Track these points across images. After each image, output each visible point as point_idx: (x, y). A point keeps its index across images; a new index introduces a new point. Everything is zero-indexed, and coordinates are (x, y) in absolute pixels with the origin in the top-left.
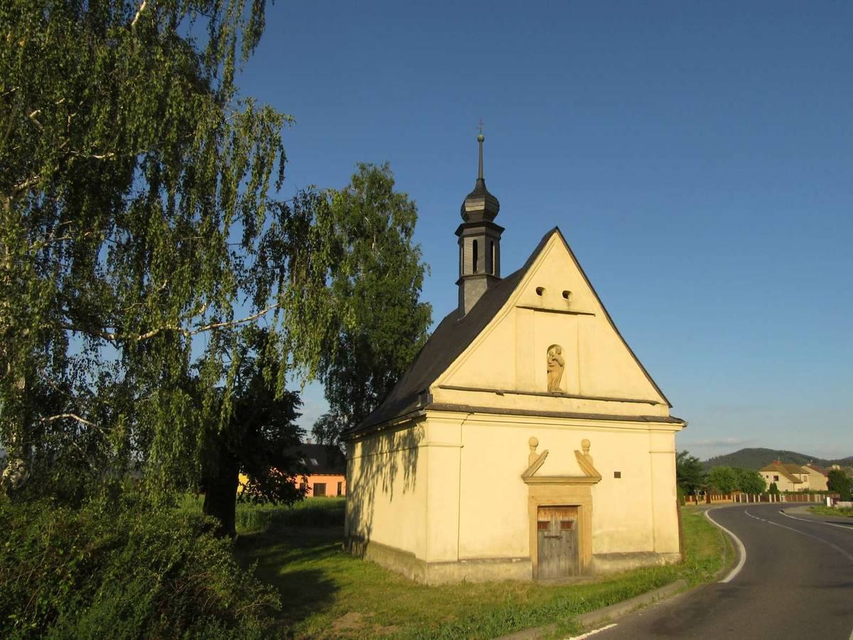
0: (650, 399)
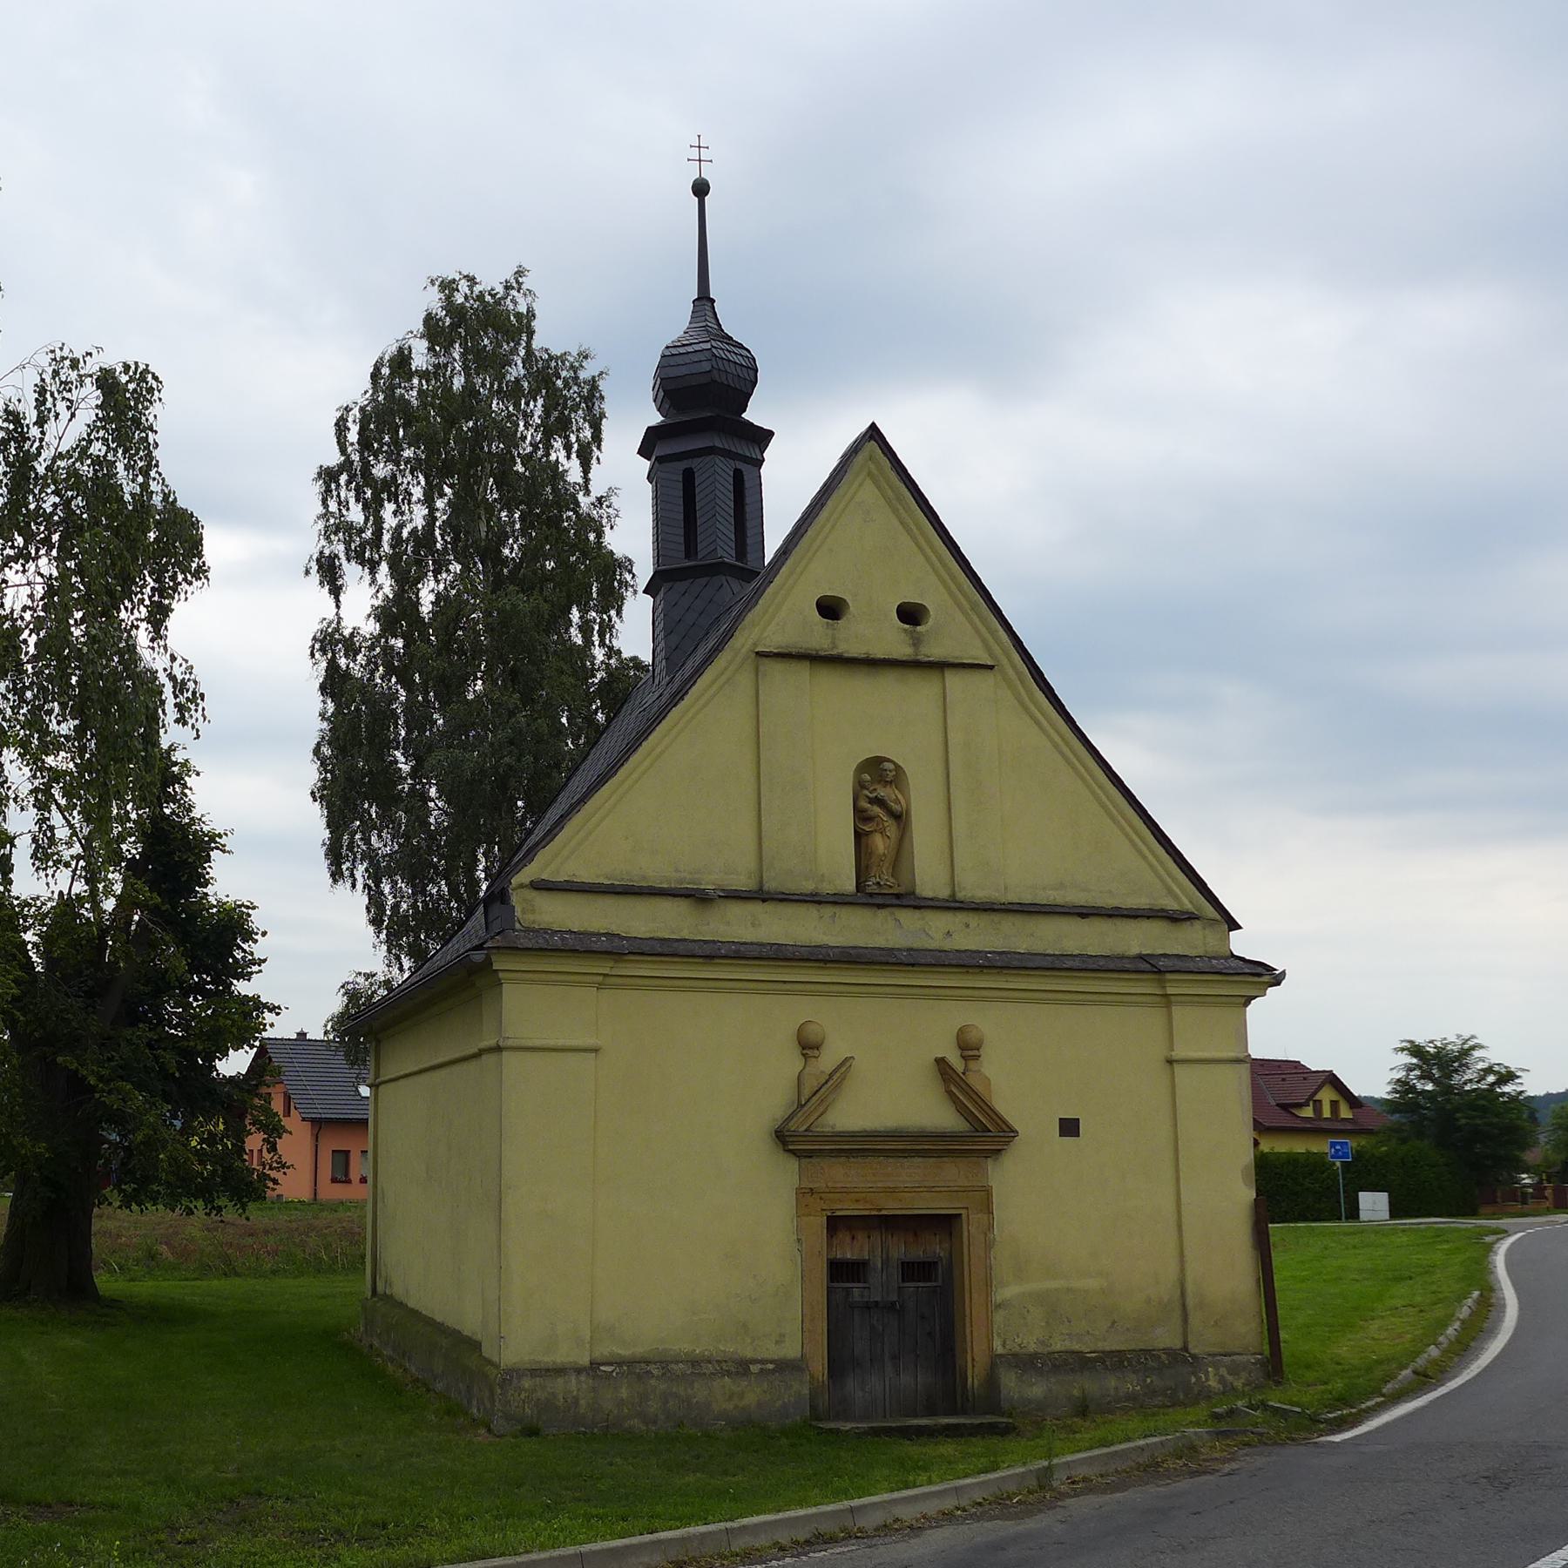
0: (1170, 904)
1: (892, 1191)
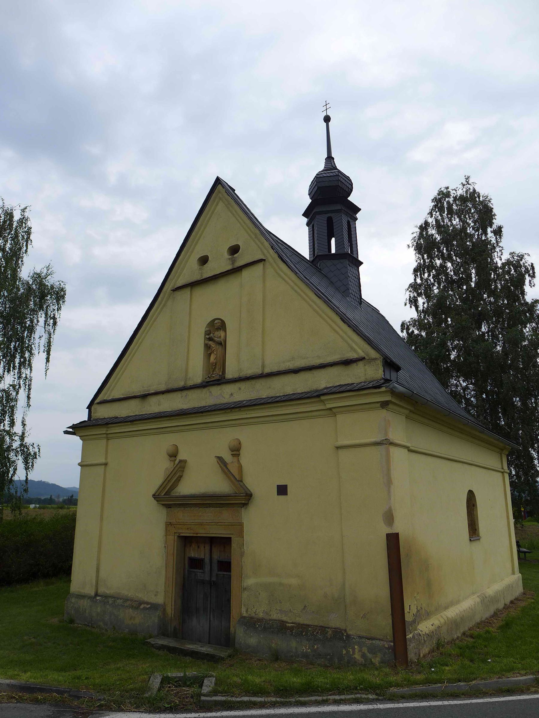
1: (201, 524)
